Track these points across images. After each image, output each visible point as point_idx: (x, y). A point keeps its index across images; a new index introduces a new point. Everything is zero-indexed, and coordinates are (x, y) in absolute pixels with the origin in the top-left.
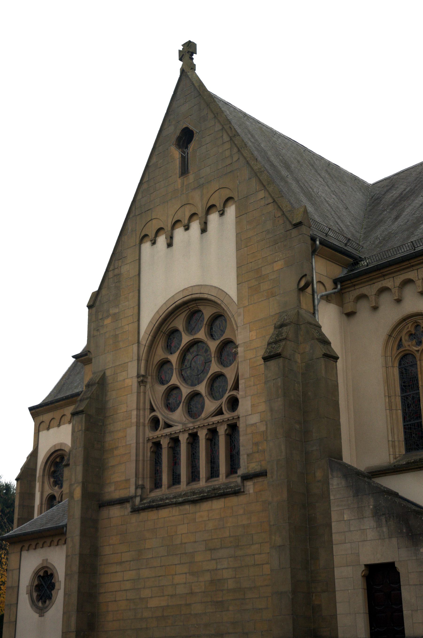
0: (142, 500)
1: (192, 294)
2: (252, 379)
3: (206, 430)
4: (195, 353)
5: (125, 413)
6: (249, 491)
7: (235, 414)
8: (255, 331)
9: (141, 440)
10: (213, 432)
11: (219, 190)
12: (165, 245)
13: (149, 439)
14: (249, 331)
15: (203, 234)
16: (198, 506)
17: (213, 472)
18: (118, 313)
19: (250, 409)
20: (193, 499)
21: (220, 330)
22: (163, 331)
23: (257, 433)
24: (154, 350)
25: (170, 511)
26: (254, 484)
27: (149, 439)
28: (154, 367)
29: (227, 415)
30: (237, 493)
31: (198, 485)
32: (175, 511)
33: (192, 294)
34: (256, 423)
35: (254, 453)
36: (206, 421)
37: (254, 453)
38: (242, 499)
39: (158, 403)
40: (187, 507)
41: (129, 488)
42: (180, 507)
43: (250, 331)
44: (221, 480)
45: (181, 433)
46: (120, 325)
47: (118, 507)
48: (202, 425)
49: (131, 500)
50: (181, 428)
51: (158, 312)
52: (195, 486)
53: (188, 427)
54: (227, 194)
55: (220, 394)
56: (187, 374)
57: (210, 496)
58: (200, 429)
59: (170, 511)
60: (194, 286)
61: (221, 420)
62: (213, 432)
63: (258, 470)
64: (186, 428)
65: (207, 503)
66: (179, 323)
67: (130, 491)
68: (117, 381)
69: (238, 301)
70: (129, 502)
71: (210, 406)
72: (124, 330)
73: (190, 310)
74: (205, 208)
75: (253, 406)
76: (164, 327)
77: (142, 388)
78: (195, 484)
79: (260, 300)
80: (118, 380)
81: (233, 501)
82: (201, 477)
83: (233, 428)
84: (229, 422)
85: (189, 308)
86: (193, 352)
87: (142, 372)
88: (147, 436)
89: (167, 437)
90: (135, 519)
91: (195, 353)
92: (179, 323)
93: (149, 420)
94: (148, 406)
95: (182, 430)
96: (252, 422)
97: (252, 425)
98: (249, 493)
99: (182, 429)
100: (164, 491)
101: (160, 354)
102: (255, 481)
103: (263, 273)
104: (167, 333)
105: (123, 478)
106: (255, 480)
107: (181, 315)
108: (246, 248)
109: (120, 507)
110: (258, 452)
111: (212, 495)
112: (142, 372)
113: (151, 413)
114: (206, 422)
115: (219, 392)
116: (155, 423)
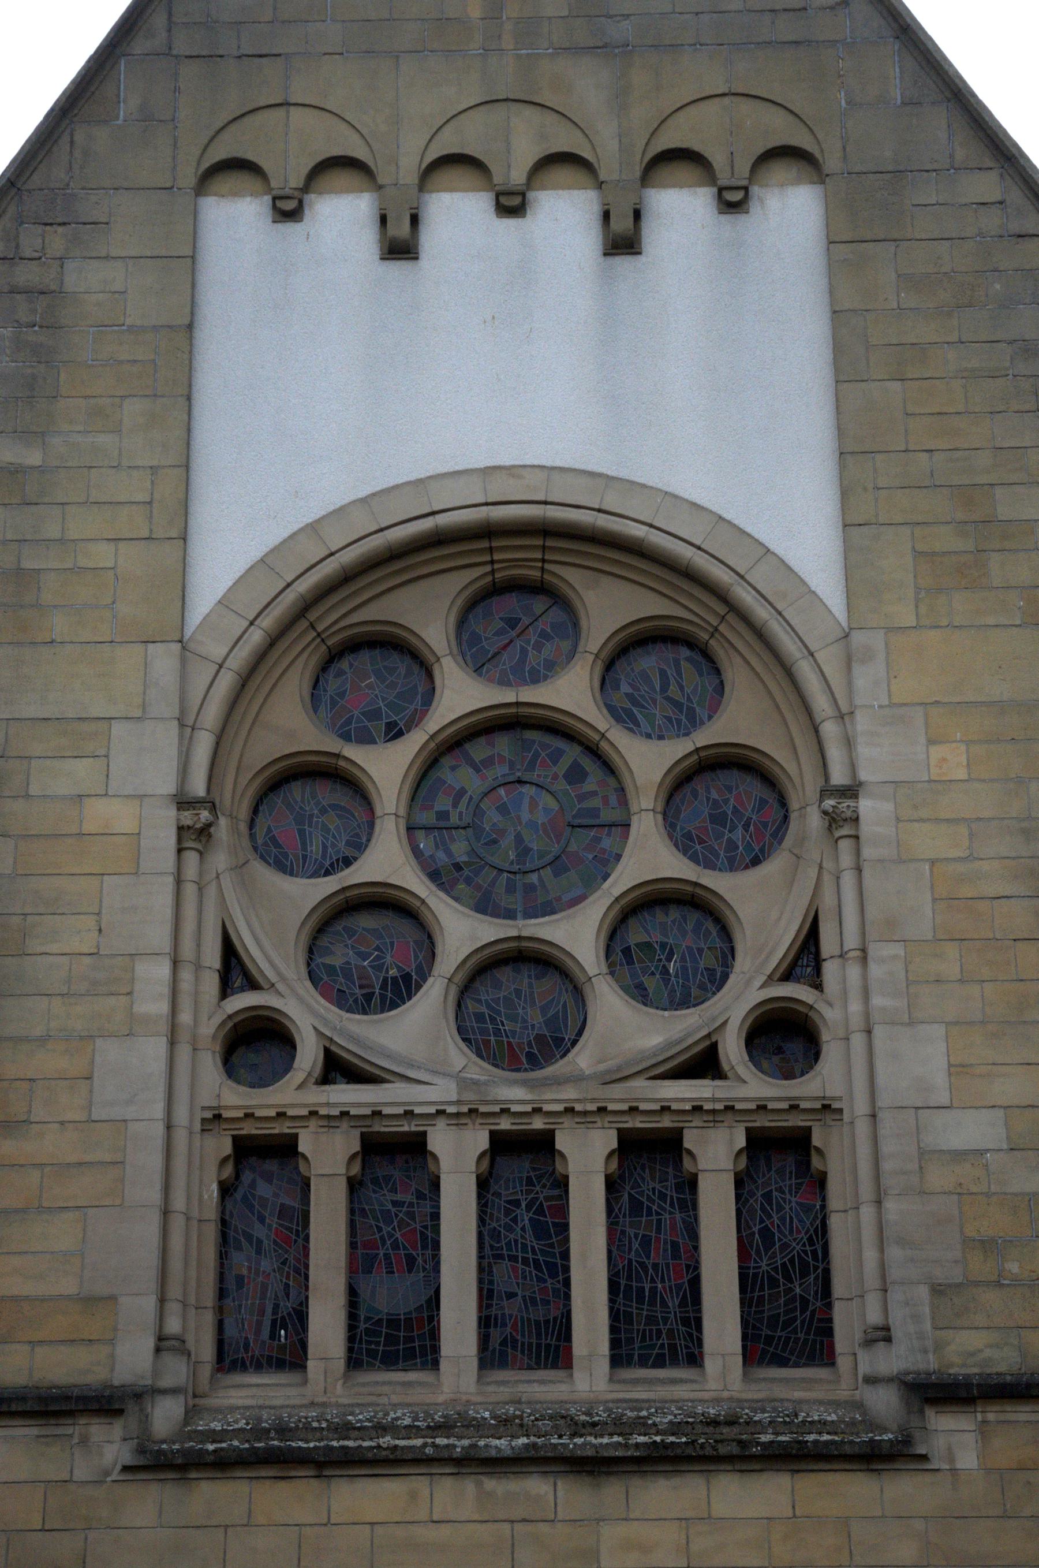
0: (191, 1413)
1: (546, 503)
2: (952, 951)
3: (486, 1135)
4: (506, 769)
5: (87, 960)
6: (952, 1460)
7: (807, 1088)
8: (963, 747)
9: (181, 1115)
10: (650, 1155)
11: (726, 100)
12: (365, 241)
13: (218, 1117)
14: (923, 740)
15: (618, 261)
16: (613, 1491)
17: (630, 1341)
18: (40, 469)
19: (940, 1079)
20: (590, 1452)
21: (669, 699)
22: (320, 628)
23: (987, 1195)
24: (260, 700)
25: (413, 1496)
26: (984, 1431)
27: (218, 1117)
28: (244, 780)
29: (749, 1084)
30: (883, 1455)
31: (563, 1387)
32: (452, 1497)
33: (546, 503)
34: (981, 1152)
35: (977, 1284)
36: (617, 1091)
37: (977, 1284)
38: (900, 1489)
39: (276, 957)
40: (537, 1486)
41: (112, 1342)
42: (490, 1484)
43: (931, 742)
44: (712, 1385)
45: (313, 1123)
46: (53, 531)
47: (26, 1431)
48: (592, 1107)
49: (131, 1407)
50: (454, 1097)
51: (313, 528)
52: (536, 1388)
53: (496, 1102)
54: (782, 131)
55: (667, 982)
56: (449, 853)
57: (709, 1451)
58: (567, 1121)
59: (413, 1496)
60: (561, 469)
61: (714, 1100)
62: (650, 1155)
63: (1002, 1368)
64: (487, 1103)
65: (676, 1481)
66: (429, 613)
67: (112, 1356)
68: (27, 796)
69: (850, 595)
70: (120, 1412)
71: (623, 1029)
72: (83, 562)
73: (493, 572)
74: (638, 157)
75: (957, 1070)
76: (328, 611)
77: (191, 858)
78: (542, 1382)
79: (991, 621)
80: (34, 790)
81: (853, 1491)
82: (447, 1348)
83: (783, 1155)
84: (762, 1121)
85: (492, 562)
86: (488, 762)
87: (198, 787)
88: (206, 1099)
89: (345, 1124)
90: (149, 1504)
91: (500, 771)
92: (608, 607)
93: (223, 1023)
94: (213, 957)
95: (451, 1109)
96: (957, 1141)
97: (959, 1156)
98: (954, 1471)
99: (458, 1102)
100: (325, 1384)
101: (290, 725)
102: (991, 1417)
103: (1004, 512)
104: (329, 643)
105: (68, 1286)
106: (992, 1413)
107: (455, 575)
108: (897, 386)
109: (35, 1431)
110: (998, 1284)
111: (723, 1450)
112: (198, 787)
113: (226, 989)
114: (617, 1097)
115: (665, 971)
116: (256, 1042)
